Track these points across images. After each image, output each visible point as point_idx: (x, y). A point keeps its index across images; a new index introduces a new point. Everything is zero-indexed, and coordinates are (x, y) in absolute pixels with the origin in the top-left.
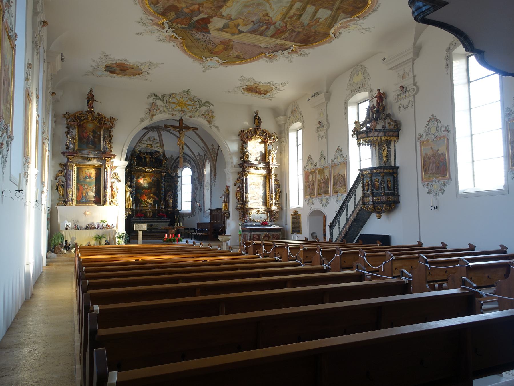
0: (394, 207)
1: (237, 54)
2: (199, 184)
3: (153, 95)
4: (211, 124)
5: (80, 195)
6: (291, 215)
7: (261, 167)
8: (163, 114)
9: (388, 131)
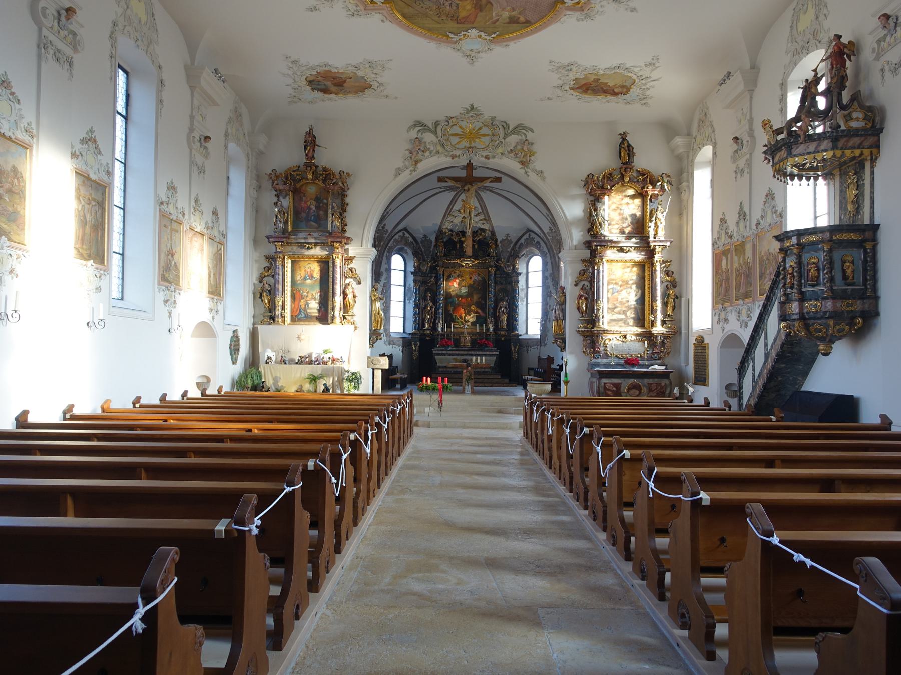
0: (860, 326)
1: (506, 15)
2: (553, 285)
3: (419, 124)
4: (528, 167)
5: (297, 307)
6: (694, 344)
7: (631, 247)
8: (435, 158)
9: (846, 136)
